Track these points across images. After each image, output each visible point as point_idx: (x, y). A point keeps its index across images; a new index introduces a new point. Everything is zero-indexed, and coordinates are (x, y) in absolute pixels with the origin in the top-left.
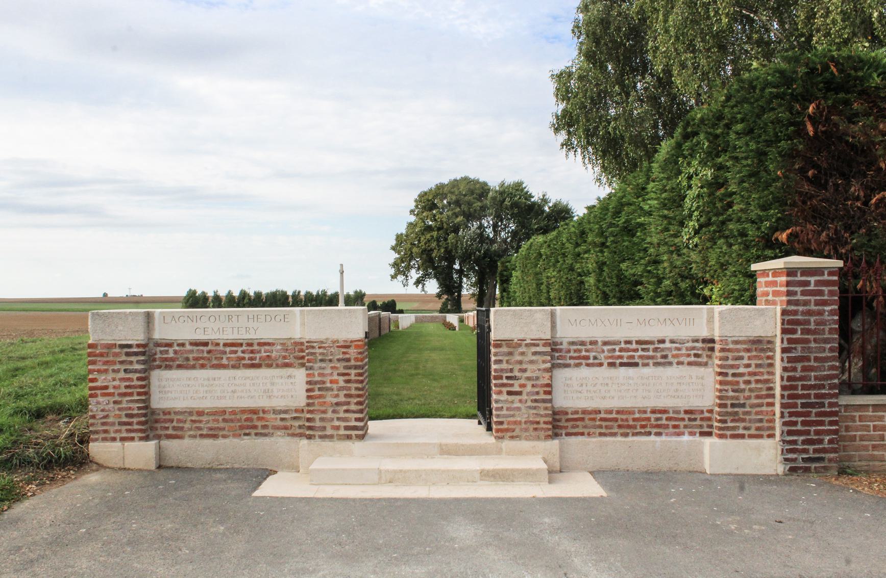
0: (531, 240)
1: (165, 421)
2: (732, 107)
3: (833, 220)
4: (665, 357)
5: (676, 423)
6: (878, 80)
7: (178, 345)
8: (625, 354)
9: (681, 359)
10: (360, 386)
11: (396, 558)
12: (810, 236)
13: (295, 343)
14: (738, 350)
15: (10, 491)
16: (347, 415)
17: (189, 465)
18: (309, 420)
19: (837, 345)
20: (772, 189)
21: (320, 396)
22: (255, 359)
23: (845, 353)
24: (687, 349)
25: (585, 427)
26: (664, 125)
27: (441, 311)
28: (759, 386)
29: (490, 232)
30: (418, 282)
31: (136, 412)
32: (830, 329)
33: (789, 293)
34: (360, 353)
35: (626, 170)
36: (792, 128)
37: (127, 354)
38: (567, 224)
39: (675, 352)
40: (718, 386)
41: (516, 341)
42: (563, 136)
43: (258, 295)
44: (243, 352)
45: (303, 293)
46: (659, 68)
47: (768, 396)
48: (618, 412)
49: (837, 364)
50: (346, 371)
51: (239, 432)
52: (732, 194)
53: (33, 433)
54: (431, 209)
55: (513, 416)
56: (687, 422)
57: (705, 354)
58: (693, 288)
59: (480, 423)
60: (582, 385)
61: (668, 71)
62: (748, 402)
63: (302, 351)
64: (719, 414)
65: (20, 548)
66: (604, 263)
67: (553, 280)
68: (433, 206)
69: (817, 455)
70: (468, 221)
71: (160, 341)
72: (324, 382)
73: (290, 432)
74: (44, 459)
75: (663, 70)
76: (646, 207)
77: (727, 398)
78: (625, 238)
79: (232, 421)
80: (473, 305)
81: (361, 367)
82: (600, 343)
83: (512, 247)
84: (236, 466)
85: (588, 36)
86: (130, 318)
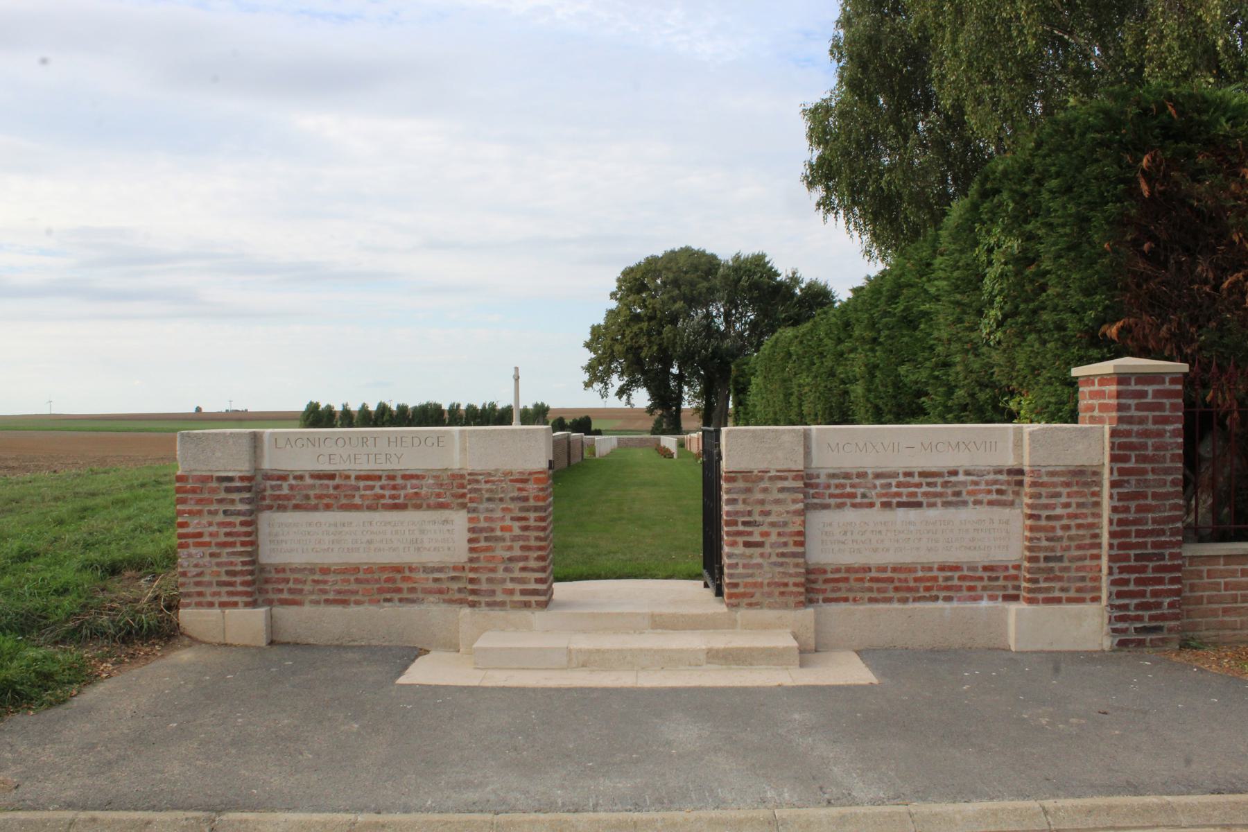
0: (777, 335)
2: (1044, 157)
3: (1175, 309)
4: (958, 494)
5: (972, 584)
6: (1227, 127)
7: (295, 478)
8: (904, 490)
9: (980, 497)
10: (542, 534)
11: (591, 768)
12: (1147, 331)
13: (453, 475)
14: (1054, 485)
15: (79, 671)
16: (524, 575)
17: (311, 641)
18: (472, 581)
19: (1181, 477)
20: (1097, 267)
21: (488, 549)
22: (398, 497)
23: (1191, 487)
24: (987, 483)
25: (850, 590)
26: (955, 180)
27: (654, 432)
28: (1081, 532)
29: (720, 323)
30: (621, 392)
31: (239, 568)
32: (1173, 455)
33: (1120, 407)
35: (905, 239)
36: (1121, 186)
37: (228, 490)
38: (825, 313)
39: (970, 488)
40: (1027, 534)
41: (756, 472)
42: (819, 193)
43: (403, 409)
44: (382, 488)
45: (463, 407)
46: (947, 103)
47: (1093, 546)
48: (894, 570)
49: (1181, 502)
50: (523, 514)
52: (1046, 273)
53: (107, 595)
54: (639, 292)
55: (752, 575)
56: (986, 583)
57: (1010, 489)
58: (995, 401)
59: (706, 586)
60: (845, 533)
61: (958, 107)
62: (1066, 554)
63: (463, 486)
64: (1029, 570)
65: (93, 746)
66: (876, 366)
67: (807, 389)
68: (642, 287)
69: (1154, 624)
70: (690, 308)
71: (270, 473)
72: (492, 530)
73: (446, 597)
74: (121, 629)
75: (952, 106)
76: (933, 290)
77: (1039, 549)
78: (905, 332)
79: (367, 581)
80: (698, 423)
81: (544, 509)
82: (870, 476)
83: (751, 344)
84: (374, 642)
85: (851, 59)
86: (231, 441)
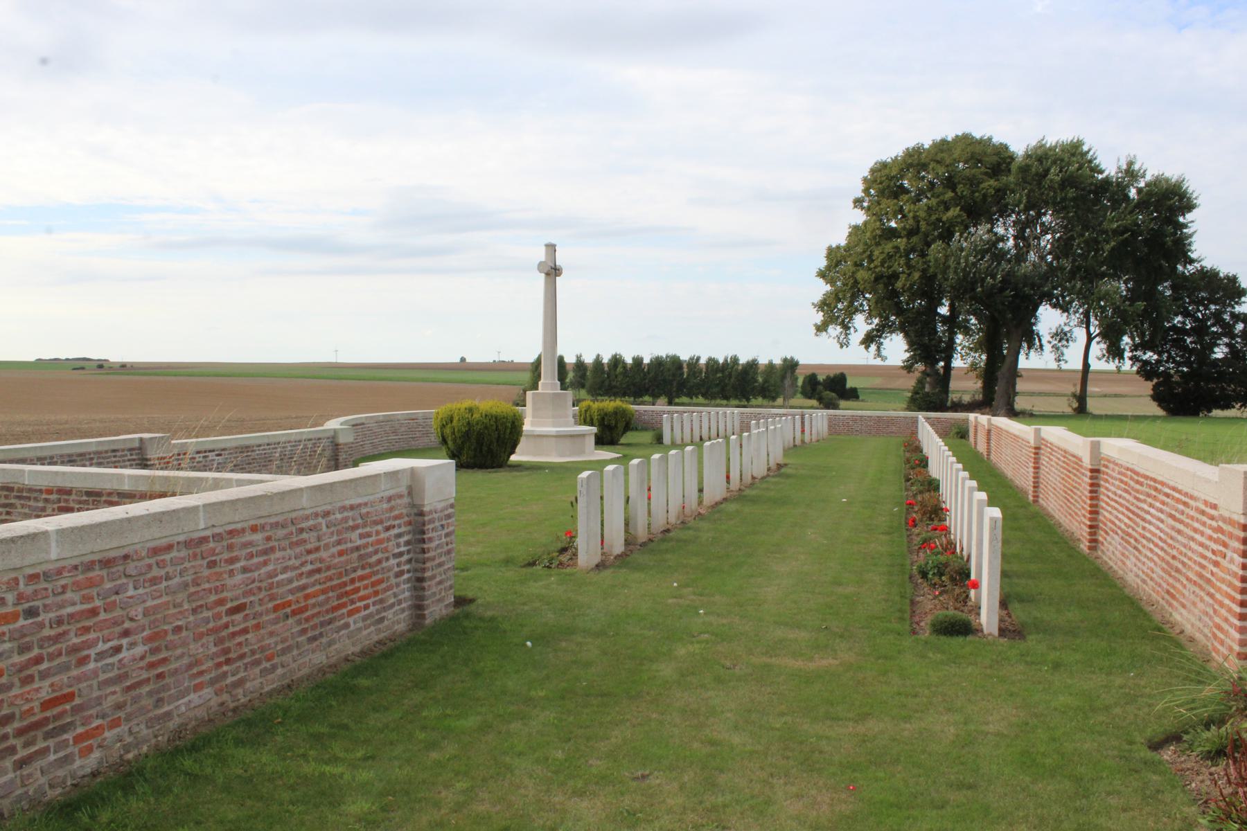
30: (869, 340)
45: (703, 361)
54: (895, 195)
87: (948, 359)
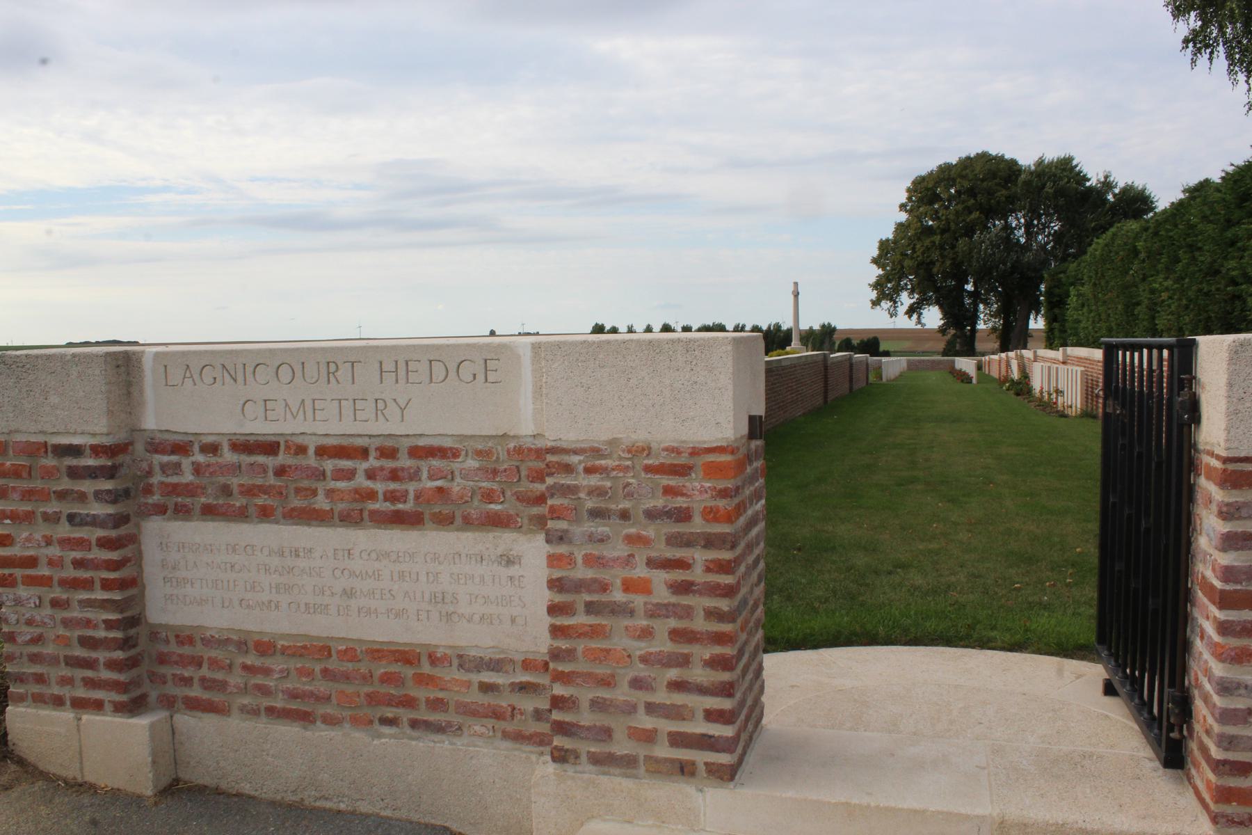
1: (184, 661)
10: (724, 605)
13: (519, 451)
16: (679, 698)
21: (595, 632)
22: (403, 497)
27: (945, 353)
30: (911, 311)
31: (101, 633)
34: (724, 494)
37: (74, 473)
44: (371, 475)
51: (368, 712)
54: (931, 203)
68: (935, 198)
72: (604, 588)
73: (510, 727)
79: (347, 677)
84: (364, 807)
87: (974, 324)
